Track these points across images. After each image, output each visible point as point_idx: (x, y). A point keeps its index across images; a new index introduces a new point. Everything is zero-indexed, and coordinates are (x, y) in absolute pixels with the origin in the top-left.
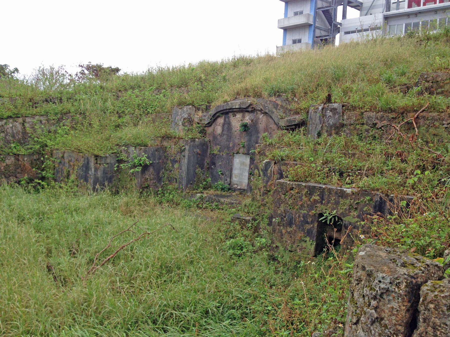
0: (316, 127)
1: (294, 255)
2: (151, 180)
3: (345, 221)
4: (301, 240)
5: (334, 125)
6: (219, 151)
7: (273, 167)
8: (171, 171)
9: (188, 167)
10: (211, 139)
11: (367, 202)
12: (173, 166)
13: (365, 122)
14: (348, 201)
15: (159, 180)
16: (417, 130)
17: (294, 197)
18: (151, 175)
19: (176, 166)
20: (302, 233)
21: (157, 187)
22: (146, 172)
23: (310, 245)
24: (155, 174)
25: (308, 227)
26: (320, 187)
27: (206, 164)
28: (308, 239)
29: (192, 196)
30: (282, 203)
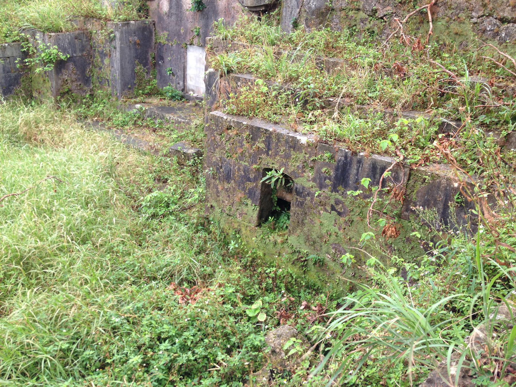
0: (291, 13)
1: (233, 220)
2: (72, 81)
3: (297, 184)
4: (241, 203)
5: (318, 9)
6: (168, 40)
7: (219, 82)
8: (101, 68)
9: (121, 65)
10: (156, 20)
11: (327, 160)
12: (102, 61)
13: (361, 7)
14: (301, 156)
15: (87, 81)
16: (431, 26)
17: (232, 140)
18: (73, 75)
19: (106, 61)
20: (243, 192)
21: (84, 91)
22: (63, 71)
23: (252, 211)
24: (78, 72)
25: (250, 185)
26: (266, 130)
27: (150, 58)
28: (249, 202)
29: (131, 107)
30: (217, 148)
